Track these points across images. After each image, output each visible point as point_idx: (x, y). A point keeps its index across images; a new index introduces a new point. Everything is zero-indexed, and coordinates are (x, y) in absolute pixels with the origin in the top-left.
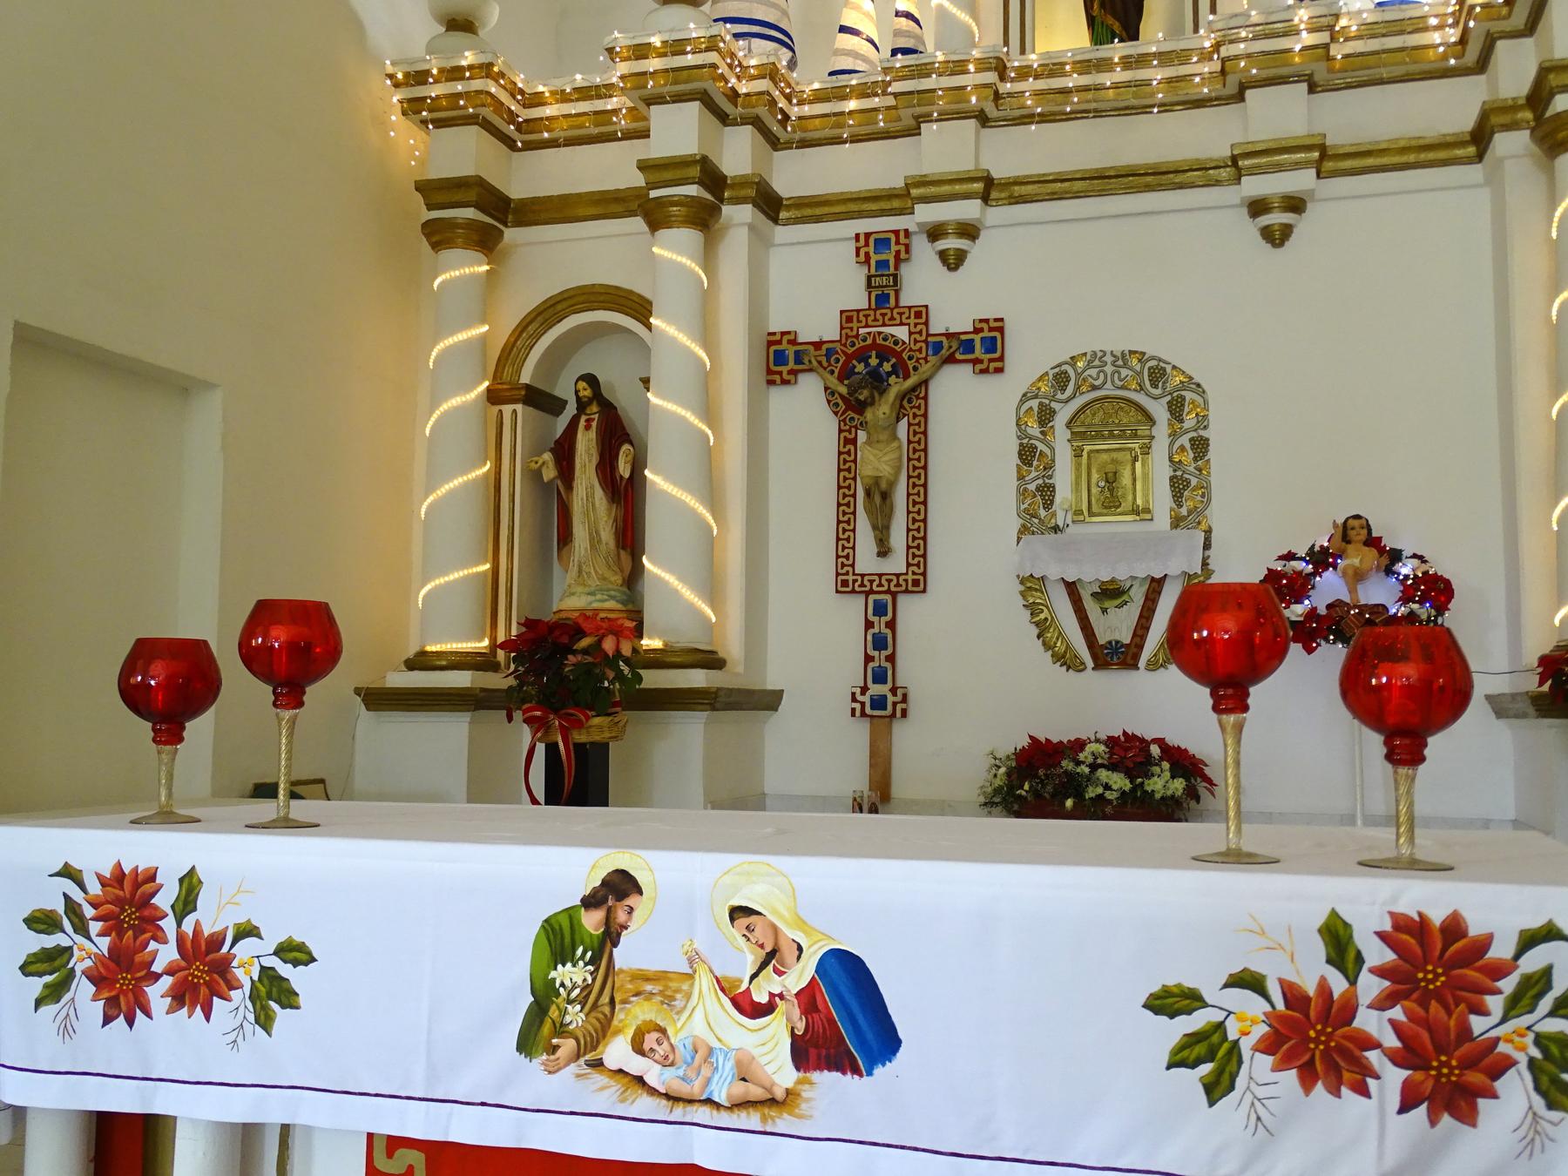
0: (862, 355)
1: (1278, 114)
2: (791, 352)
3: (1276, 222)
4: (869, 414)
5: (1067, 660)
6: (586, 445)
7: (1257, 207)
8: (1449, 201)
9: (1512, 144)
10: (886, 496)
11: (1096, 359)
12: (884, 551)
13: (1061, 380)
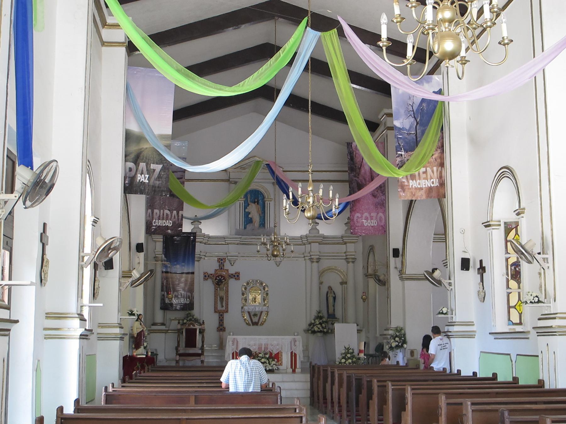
0: (218, 276)
12: (222, 307)
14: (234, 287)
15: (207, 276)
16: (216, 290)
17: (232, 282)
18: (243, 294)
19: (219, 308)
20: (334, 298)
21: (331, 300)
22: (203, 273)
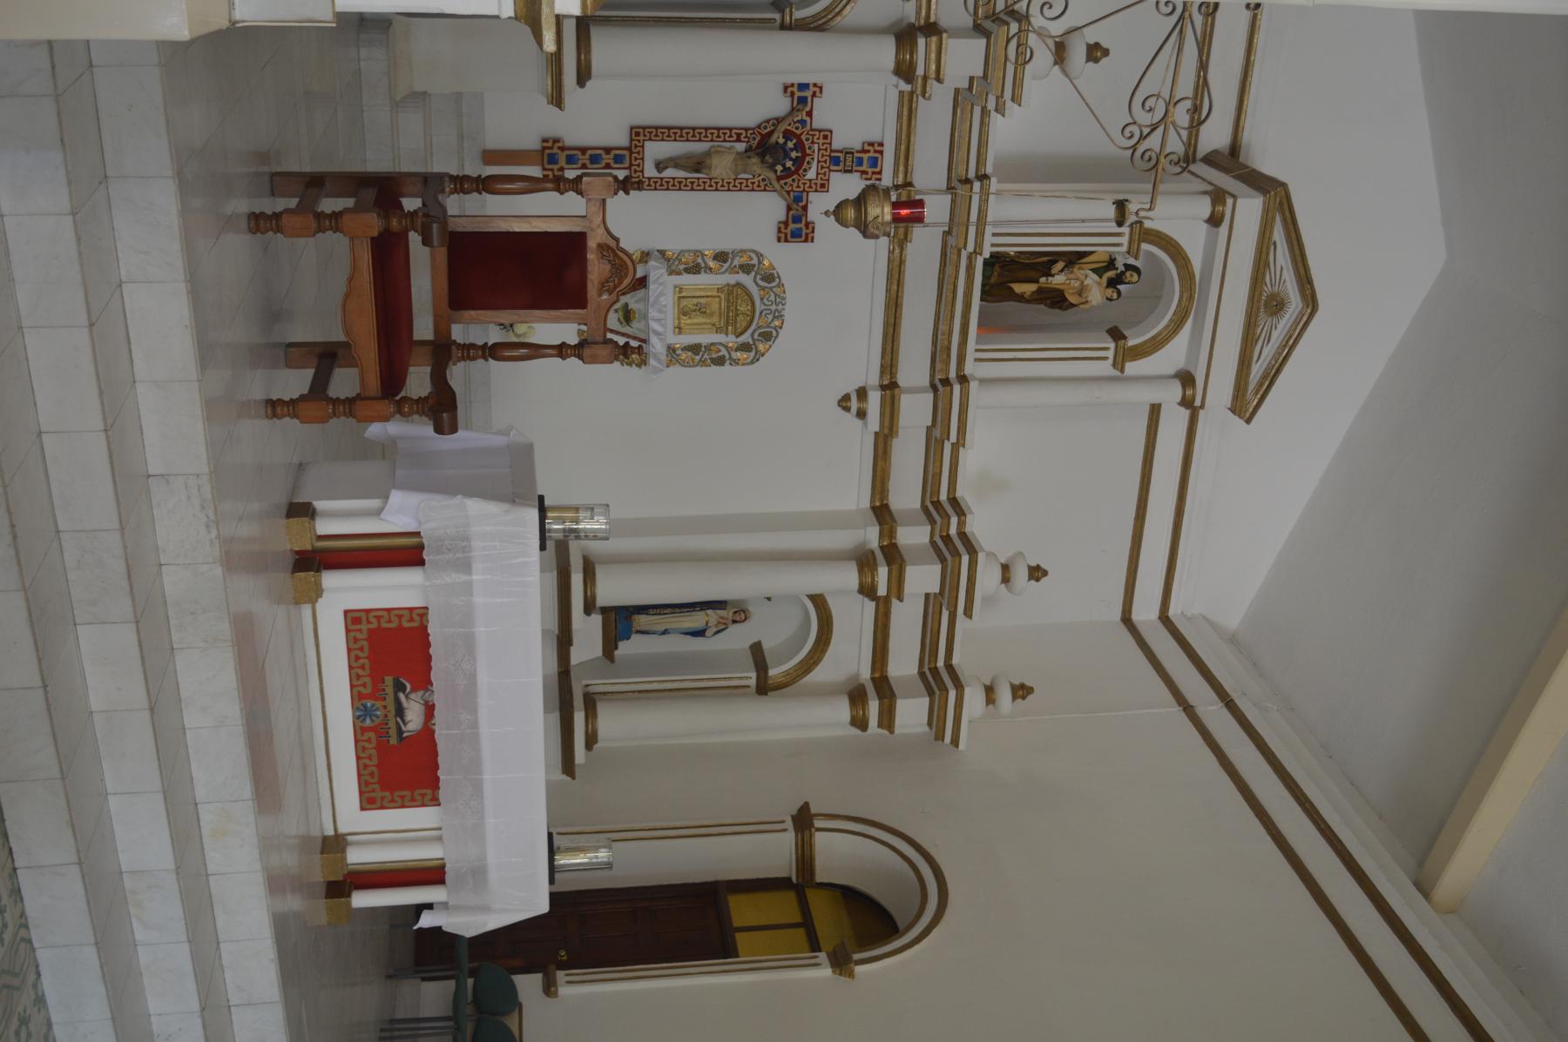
0: (799, 146)
1: (916, 411)
2: (808, 94)
4: (755, 160)
7: (862, 393)
8: (857, 497)
9: (871, 536)
10: (697, 171)
11: (781, 300)
12: (660, 166)
13: (769, 278)
14: (749, 218)
15: (802, 95)
16: (737, 134)
17: (772, 207)
18: (721, 257)
19: (655, 150)
20: (700, 633)
21: (696, 620)
22: (818, 81)
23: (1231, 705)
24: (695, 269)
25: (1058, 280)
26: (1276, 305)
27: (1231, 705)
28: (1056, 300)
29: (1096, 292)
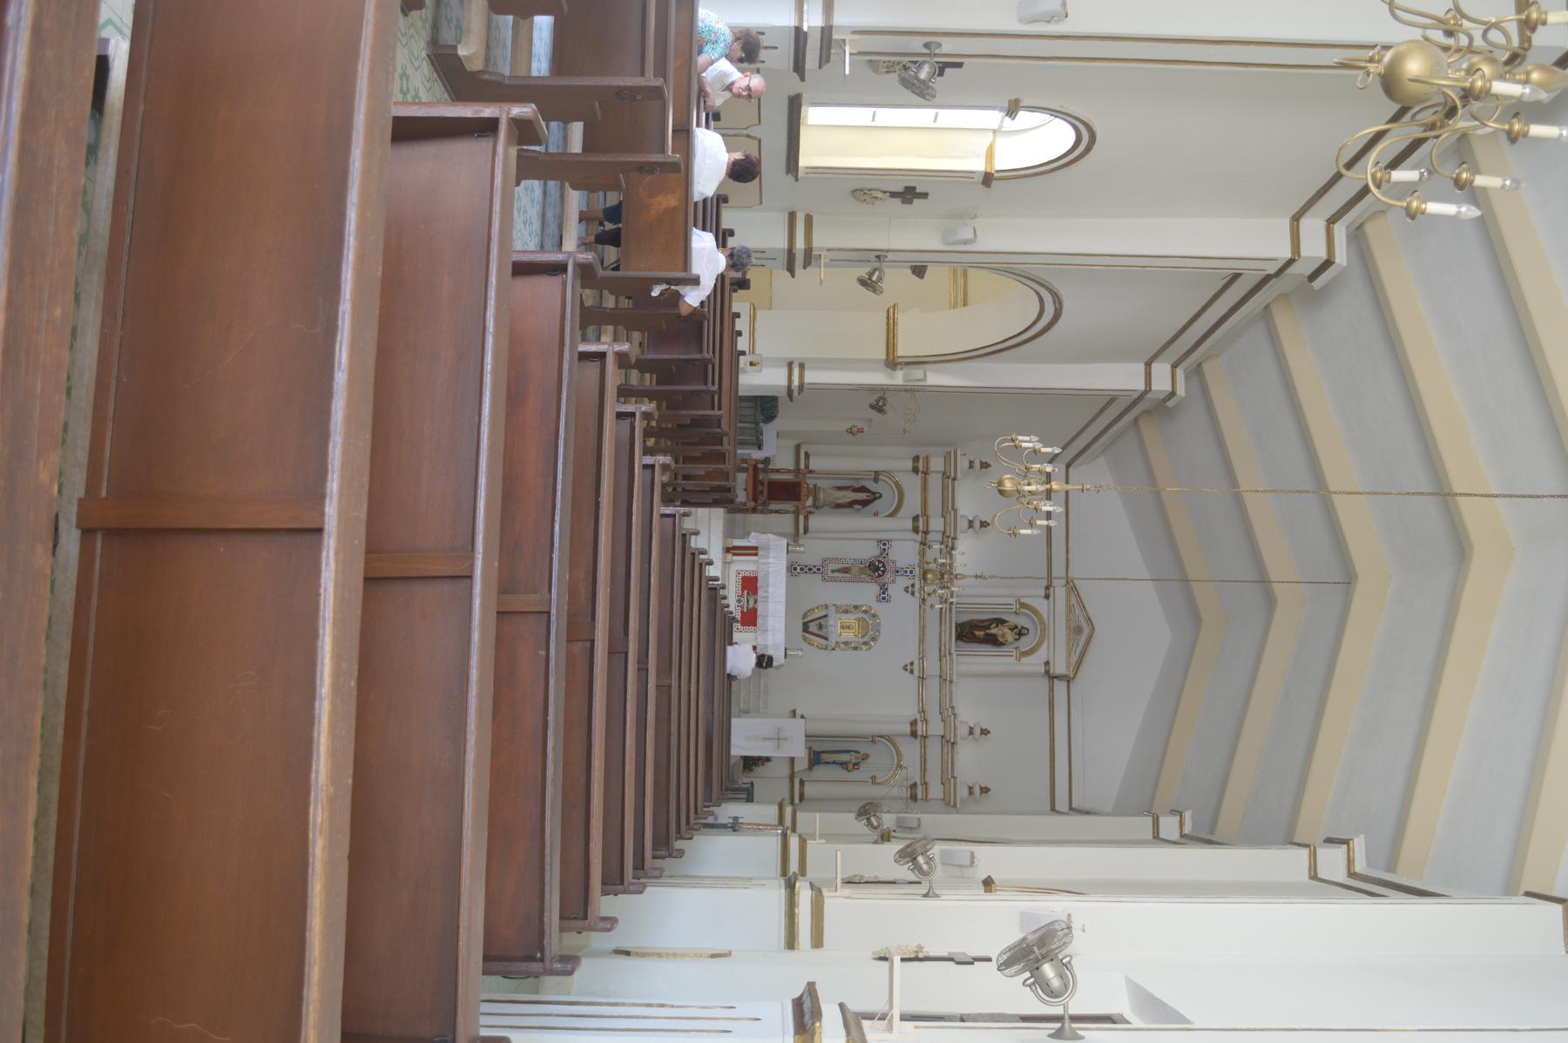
3: (909, 668)
5: (805, 616)
6: (862, 496)
14: (866, 593)
17: (874, 589)
18: (856, 607)
23: (1094, 419)
24: (846, 612)
25: (993, 631)
26: (1079, 630)
27: (1094, 419)
28: (994, 641)
29: (1010, 636)
